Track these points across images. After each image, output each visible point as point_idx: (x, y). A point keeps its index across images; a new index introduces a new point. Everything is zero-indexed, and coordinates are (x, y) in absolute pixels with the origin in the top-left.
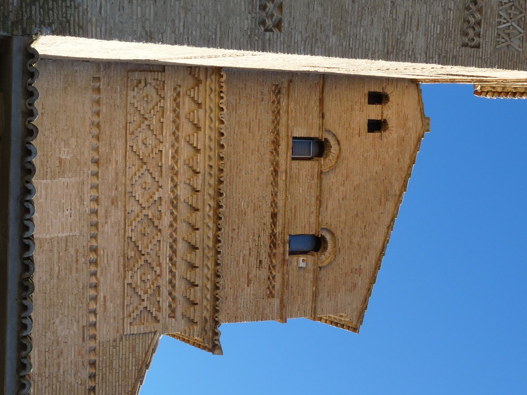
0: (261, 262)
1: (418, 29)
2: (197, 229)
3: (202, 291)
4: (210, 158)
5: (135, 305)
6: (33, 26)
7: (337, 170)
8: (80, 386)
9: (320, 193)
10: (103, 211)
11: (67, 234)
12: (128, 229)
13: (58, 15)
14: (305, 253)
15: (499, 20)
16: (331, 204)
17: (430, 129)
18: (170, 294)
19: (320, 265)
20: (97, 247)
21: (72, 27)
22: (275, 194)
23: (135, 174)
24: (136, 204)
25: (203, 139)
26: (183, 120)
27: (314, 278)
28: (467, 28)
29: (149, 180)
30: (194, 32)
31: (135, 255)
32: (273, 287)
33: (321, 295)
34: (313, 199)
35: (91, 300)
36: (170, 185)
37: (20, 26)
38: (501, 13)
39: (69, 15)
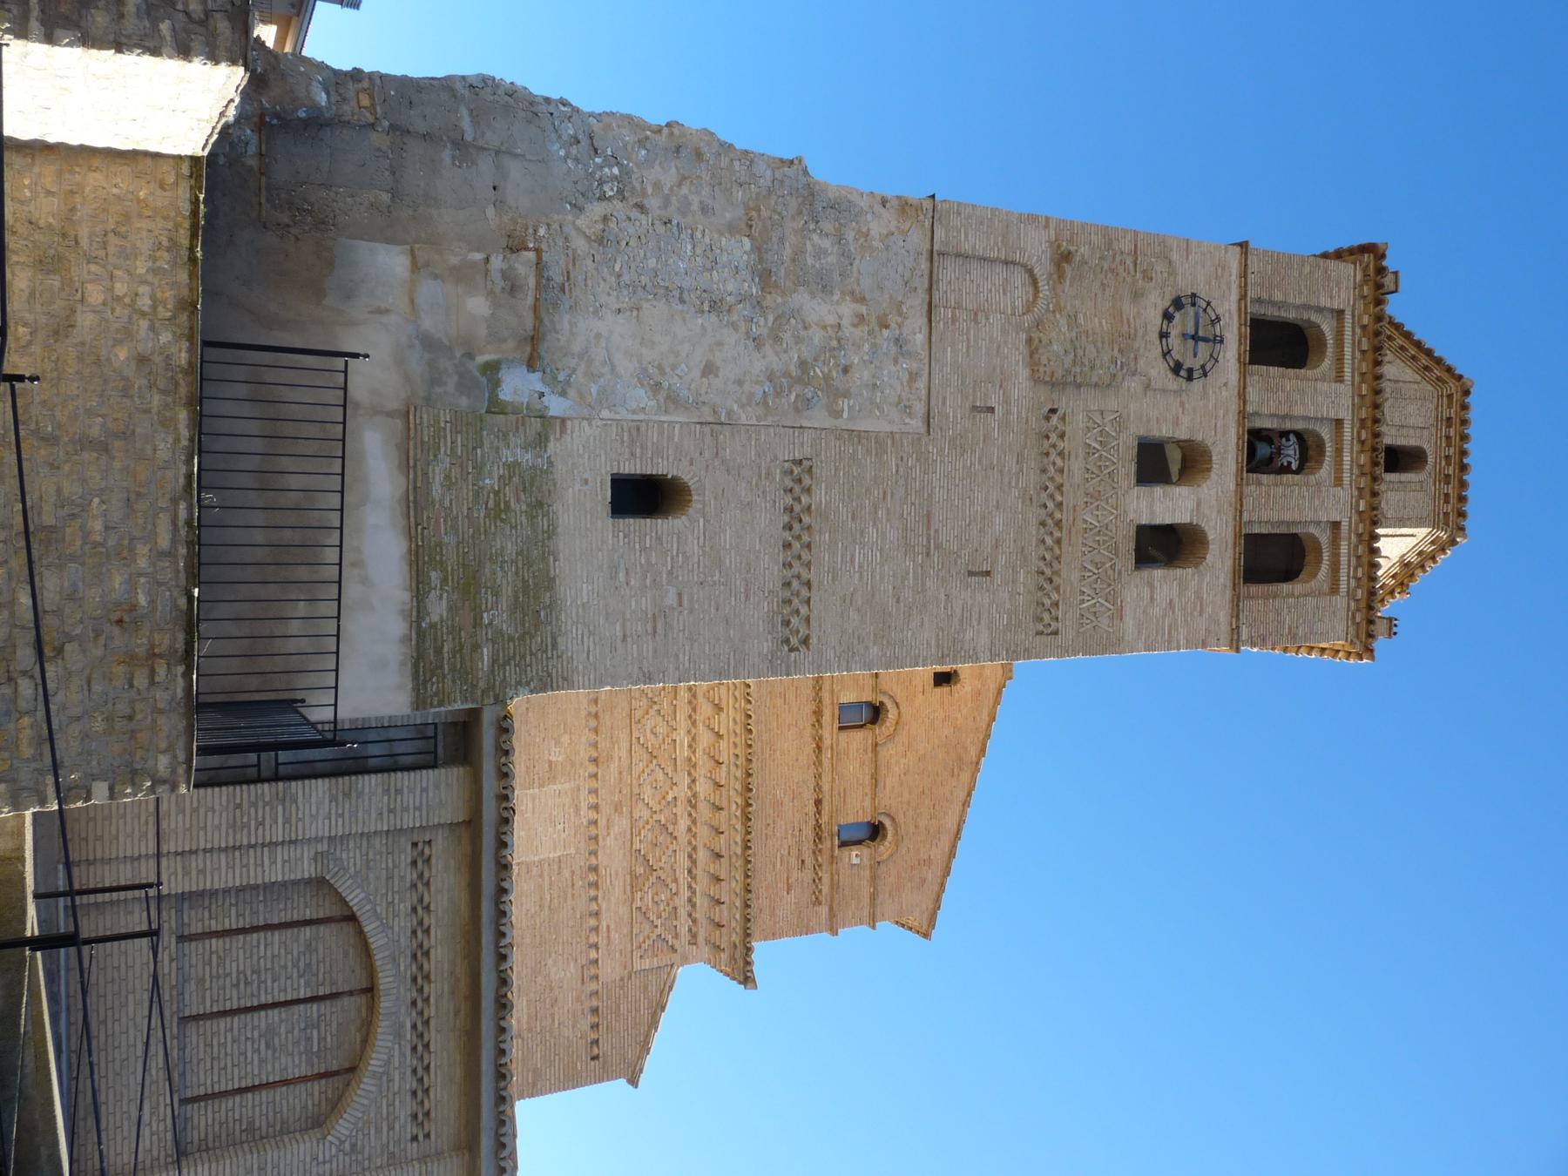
0: (803, 861)
1: (979, 623)
2: (722, 833)
3: (730, 910)
4: (735, 745)
5: (646, 933)
6: (507, 690)
7: (897, 739)
8: (580, 1041)
9: (876, 769)
10: (604, 821)
12: (636, 840)
13: (537, 670)
14: (859, 842)
15: (1082, 597)
16: (890, 781)
17: (1014, 676)
18: (690, 915)
19: (878, 859)
20: (597, 865)
21: (554, 680)
22: (818, 776)
23: (643, 772)
24: (645, 808)
25: (726, 721)
26: (701, 699)
27: (871, 877)
28: (1041, 613)
29: (661, 776)
30: (702, 666)
31: (645, 871)
32: (820, 892)
33: (881, 896)
34: (867, 778)
35: (590, 931)
36: (687, 780)
37: (491, 693)
38: (1083, 589)
39: (550, 667)
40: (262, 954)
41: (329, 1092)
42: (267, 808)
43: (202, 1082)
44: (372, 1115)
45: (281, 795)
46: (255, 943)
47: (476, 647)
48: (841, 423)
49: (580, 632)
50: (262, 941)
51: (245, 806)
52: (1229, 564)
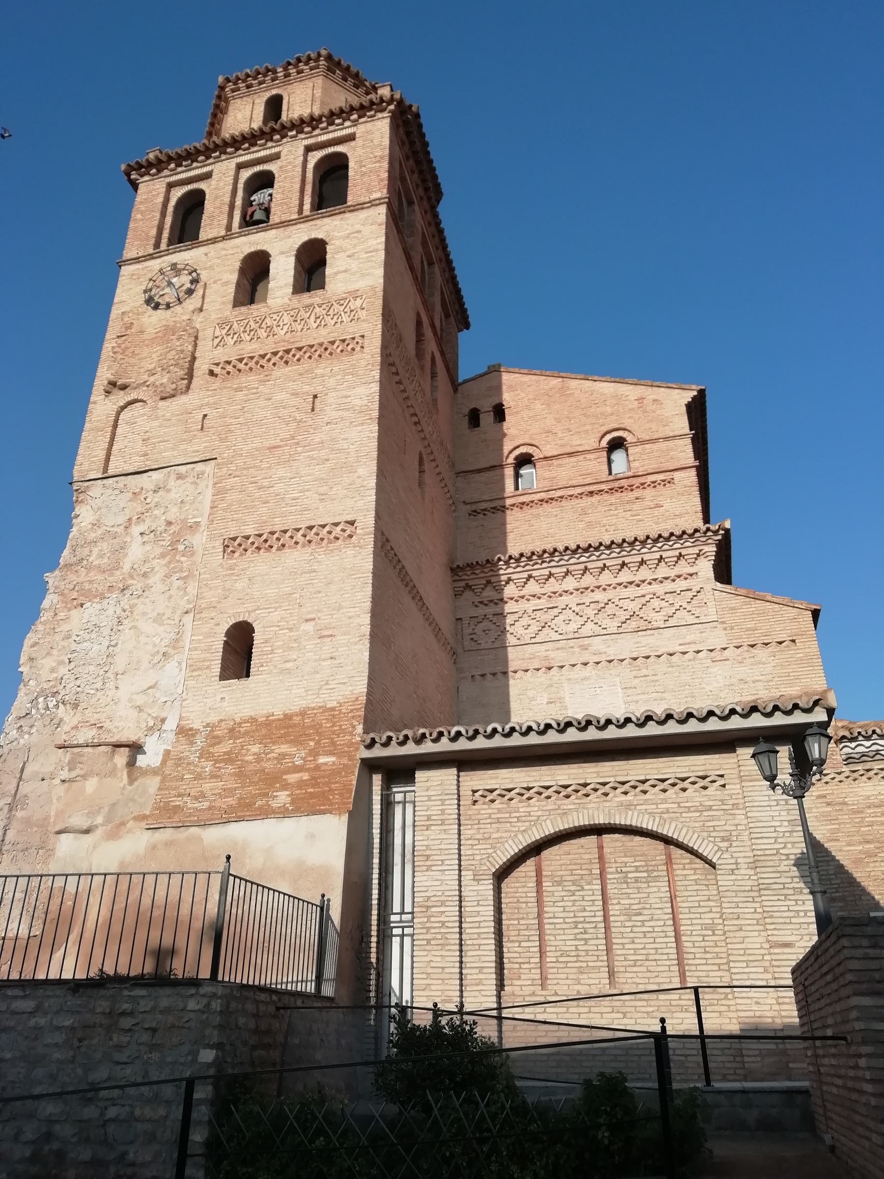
0: (637, 499)
11: (620, 689)
18: (674, 581)
34: (573, 459)
40: (561, 920)
41: (684, 861)
42: (433, 919)
43: (667, 968)
44: (697, 825)
45: (424, 910)
46: (552, 926)
47: (318, 767)
48: (204, 521)
49: (326, 692)
50: (551, 921)
51: (428, 937)
52: (326, 220)
